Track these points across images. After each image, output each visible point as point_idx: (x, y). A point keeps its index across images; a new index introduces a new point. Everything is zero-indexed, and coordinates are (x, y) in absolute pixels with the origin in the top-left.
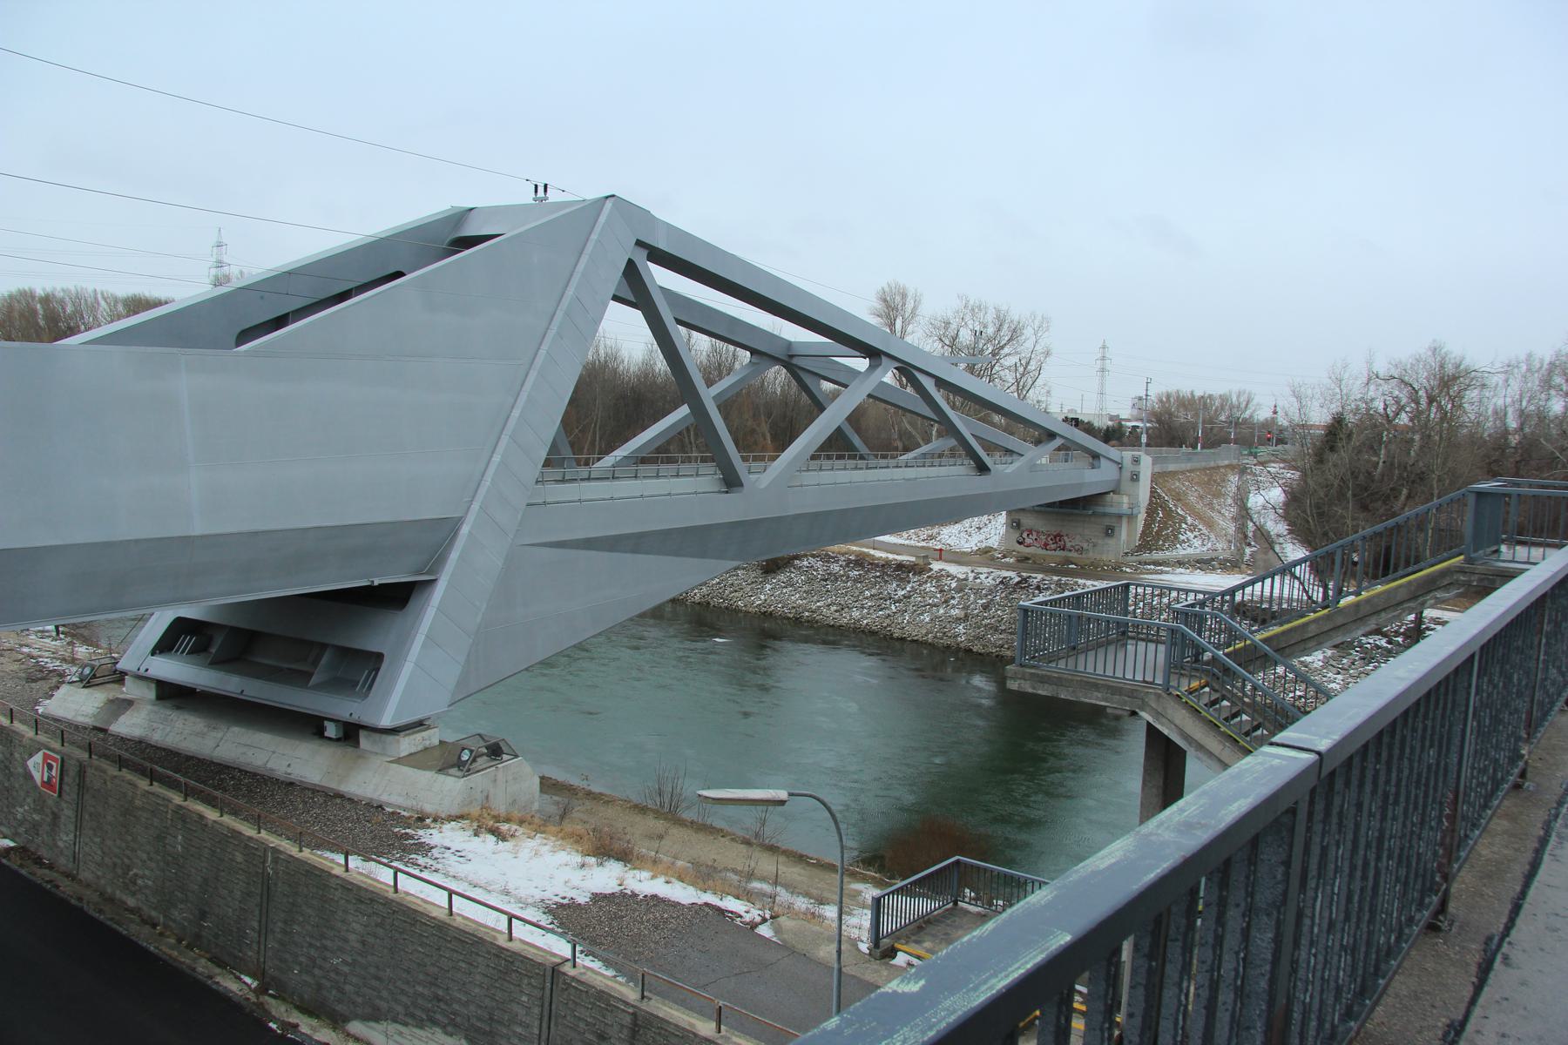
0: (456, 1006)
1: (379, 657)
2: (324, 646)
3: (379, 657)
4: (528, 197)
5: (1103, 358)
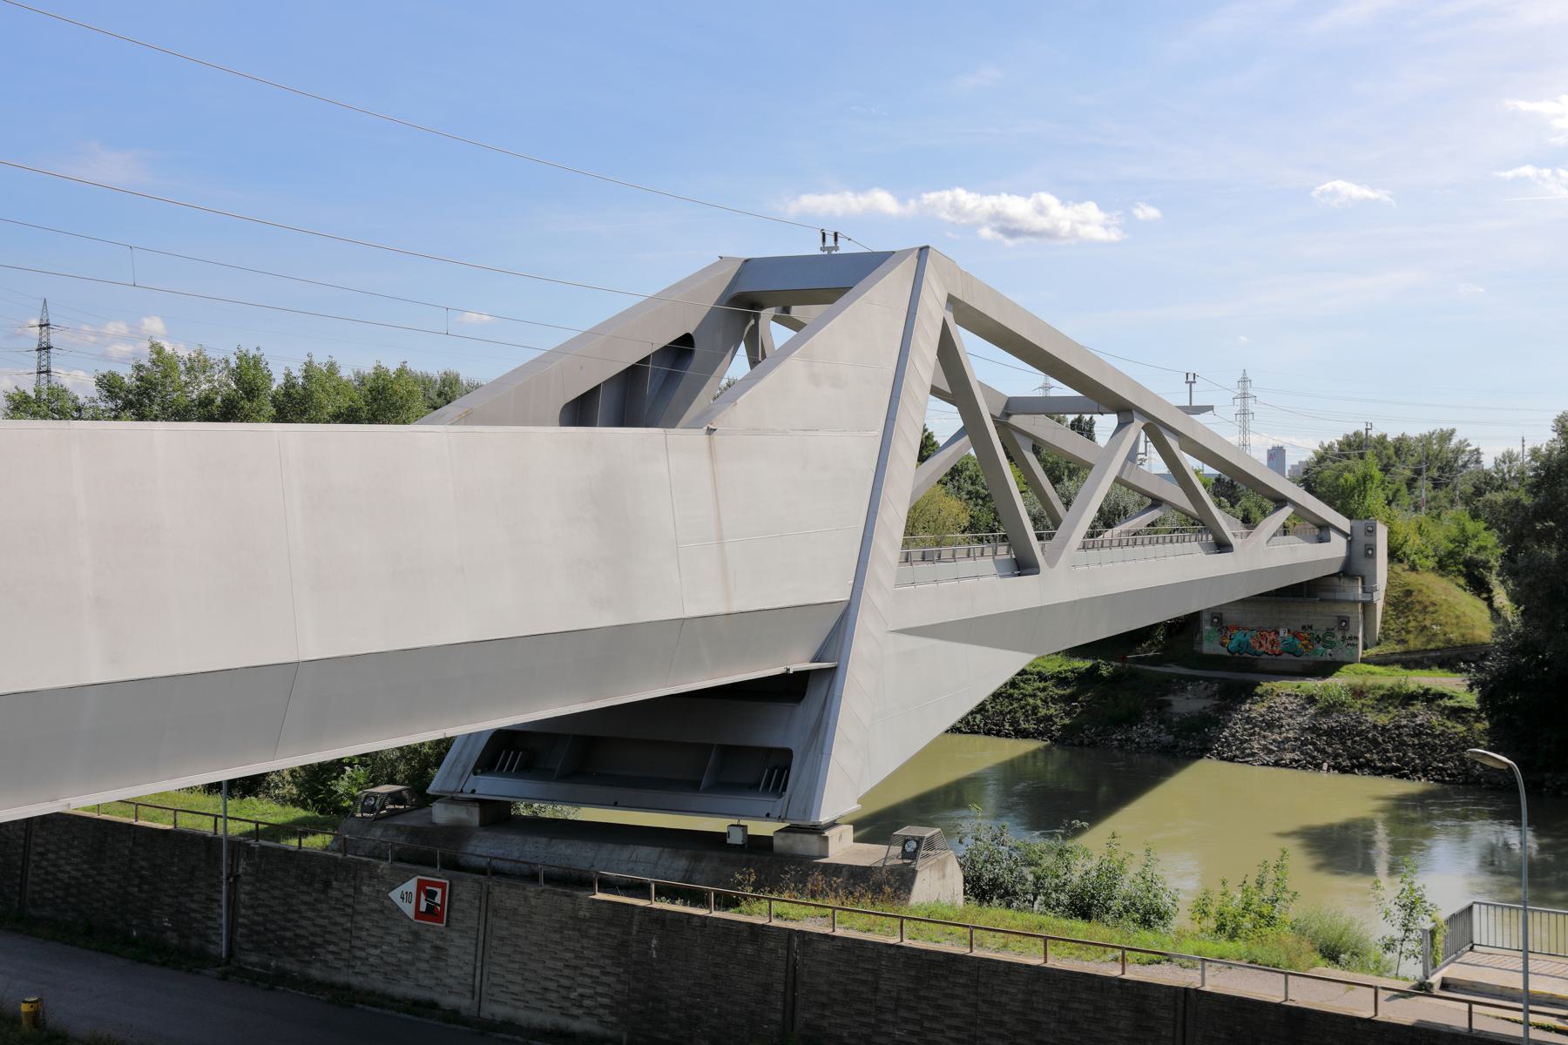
0: (927, 1024)
1: (788, 753)
2: (707, 748)
3: (788, 753)
4: (814, 249)
5: (1244, 396)
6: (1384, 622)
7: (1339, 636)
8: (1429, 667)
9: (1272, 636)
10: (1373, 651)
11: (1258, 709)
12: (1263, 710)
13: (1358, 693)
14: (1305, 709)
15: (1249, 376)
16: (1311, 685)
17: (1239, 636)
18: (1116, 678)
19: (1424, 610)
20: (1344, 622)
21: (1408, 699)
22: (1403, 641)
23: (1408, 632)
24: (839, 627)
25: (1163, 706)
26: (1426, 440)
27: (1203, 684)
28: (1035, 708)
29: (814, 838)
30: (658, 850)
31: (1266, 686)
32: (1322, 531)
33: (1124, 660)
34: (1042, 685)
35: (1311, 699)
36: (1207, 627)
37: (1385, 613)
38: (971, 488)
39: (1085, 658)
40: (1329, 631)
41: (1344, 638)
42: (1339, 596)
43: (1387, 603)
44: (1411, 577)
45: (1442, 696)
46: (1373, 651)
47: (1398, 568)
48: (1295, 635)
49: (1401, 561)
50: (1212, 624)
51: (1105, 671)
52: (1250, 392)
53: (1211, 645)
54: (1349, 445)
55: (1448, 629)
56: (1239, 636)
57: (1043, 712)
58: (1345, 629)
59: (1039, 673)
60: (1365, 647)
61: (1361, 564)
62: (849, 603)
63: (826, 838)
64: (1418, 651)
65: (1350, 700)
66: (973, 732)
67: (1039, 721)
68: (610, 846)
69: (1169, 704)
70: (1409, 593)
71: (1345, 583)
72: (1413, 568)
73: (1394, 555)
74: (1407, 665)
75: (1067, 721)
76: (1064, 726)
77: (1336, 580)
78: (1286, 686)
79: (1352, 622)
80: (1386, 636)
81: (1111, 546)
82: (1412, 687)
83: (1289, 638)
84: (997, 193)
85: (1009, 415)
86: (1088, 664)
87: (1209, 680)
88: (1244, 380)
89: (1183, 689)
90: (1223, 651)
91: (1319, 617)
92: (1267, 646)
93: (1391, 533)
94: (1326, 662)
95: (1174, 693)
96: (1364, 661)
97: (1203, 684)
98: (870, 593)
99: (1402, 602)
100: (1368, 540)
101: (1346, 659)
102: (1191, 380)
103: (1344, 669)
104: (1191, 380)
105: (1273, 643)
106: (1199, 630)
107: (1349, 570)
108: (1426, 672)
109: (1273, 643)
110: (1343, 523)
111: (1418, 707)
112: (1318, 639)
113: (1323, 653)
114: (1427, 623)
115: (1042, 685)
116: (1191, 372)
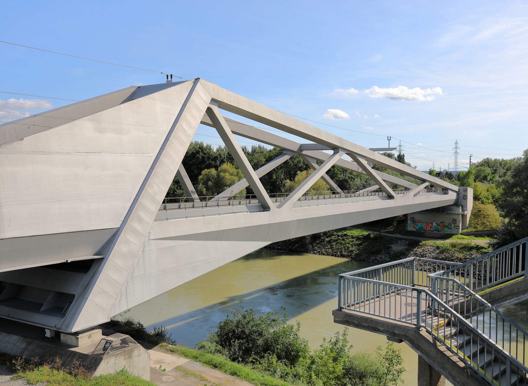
3: (73, 296)
5: (456, 148)
6: (470, 221)
7: (453, 225)
8: (484, 237)
9: (431, 225)
10: (465, 231)
11: (419, 250)
12: (421, 251)
13: (453, 246)
14: (435, 251)
15: (458, 142)
16: (439, 242)
17: (420, 225)
18: (376, 238)
19: (484, 217)
20: (455, 221)
21: (470, 248)
22: (476, 228)
23: (478, 224)
24: (110, 240)
25: (389, 248)
26: (511, 161)
27: (403, 241)
28: (348, 247)
29: (73, 337)
30: (19, 337)
31: (424, 242)
32: (445, 190)
33: (380, 232)
34: (352, 240)
35: (438, 248)
36: (409, 222)
37: (471, 218)
38: (349, 175)
39: (367, 230)
40: (450, 224)
41: (455, 226)
42: (453, 212)
43: (472, 214)
44: (482, 206)
45: (482, 248)
46: (465, 231)
47: (477, 203)
48: (438, 225)
49: (479, 200)
50: (411, 221)
51: (372, 236)
52: (458, 146)
53: (410, 227)
54: (485, 162)
55: (492, 224)
56: (420, 225)
57: (351, 249)
58: (455, 223)
59: (352, 236)
60: (462, 229)
61: (462, 201)
62: (119, 229)
63: (78, 338)
64: (481, 231)
65: (451, 248)
66: (328, 255)
67: (349, 252)
68: (4, 334)
69: (391, 247)
70: (480, 211)
71: (455, 208)
72: (483, 203)
73: (476, 198)
74: (476, 236)
75: (357, 252)
76: (356, 254)
77: (452, 207)
78: (431, 242)
79: (457, 221)
80: (470, 225)
81: (363, 196)
82: (473, 244)
83: (436, 226)
84: (389, 88)
85: (302, 151)
86: (367, 233)
87: (406, 239)
88: (456, 143)
89: (397, 243)
90: (414, 230)
91: (446, 219)
92: (429, 228)
93: (475, 191)
94: (449, 234)
95: (394, 244)
96: (461, 234)
97: (403, 241)
98: (133, 223)
99: (476, 214)
100: (465, 193)
101: (456, 233)
102: (389, 139)
103: (454, 237)
104: (389, 139)
105: (431, 227)
106: (407, 222)
107: (457, 204)
108: (483, 238)
109: (431, 227)
110: (456, 188)
111: (474, 251)
112: (446, 227)
113: (447, 231)
114: (485, 221)
115: (352, 240)
116: (389, 136)
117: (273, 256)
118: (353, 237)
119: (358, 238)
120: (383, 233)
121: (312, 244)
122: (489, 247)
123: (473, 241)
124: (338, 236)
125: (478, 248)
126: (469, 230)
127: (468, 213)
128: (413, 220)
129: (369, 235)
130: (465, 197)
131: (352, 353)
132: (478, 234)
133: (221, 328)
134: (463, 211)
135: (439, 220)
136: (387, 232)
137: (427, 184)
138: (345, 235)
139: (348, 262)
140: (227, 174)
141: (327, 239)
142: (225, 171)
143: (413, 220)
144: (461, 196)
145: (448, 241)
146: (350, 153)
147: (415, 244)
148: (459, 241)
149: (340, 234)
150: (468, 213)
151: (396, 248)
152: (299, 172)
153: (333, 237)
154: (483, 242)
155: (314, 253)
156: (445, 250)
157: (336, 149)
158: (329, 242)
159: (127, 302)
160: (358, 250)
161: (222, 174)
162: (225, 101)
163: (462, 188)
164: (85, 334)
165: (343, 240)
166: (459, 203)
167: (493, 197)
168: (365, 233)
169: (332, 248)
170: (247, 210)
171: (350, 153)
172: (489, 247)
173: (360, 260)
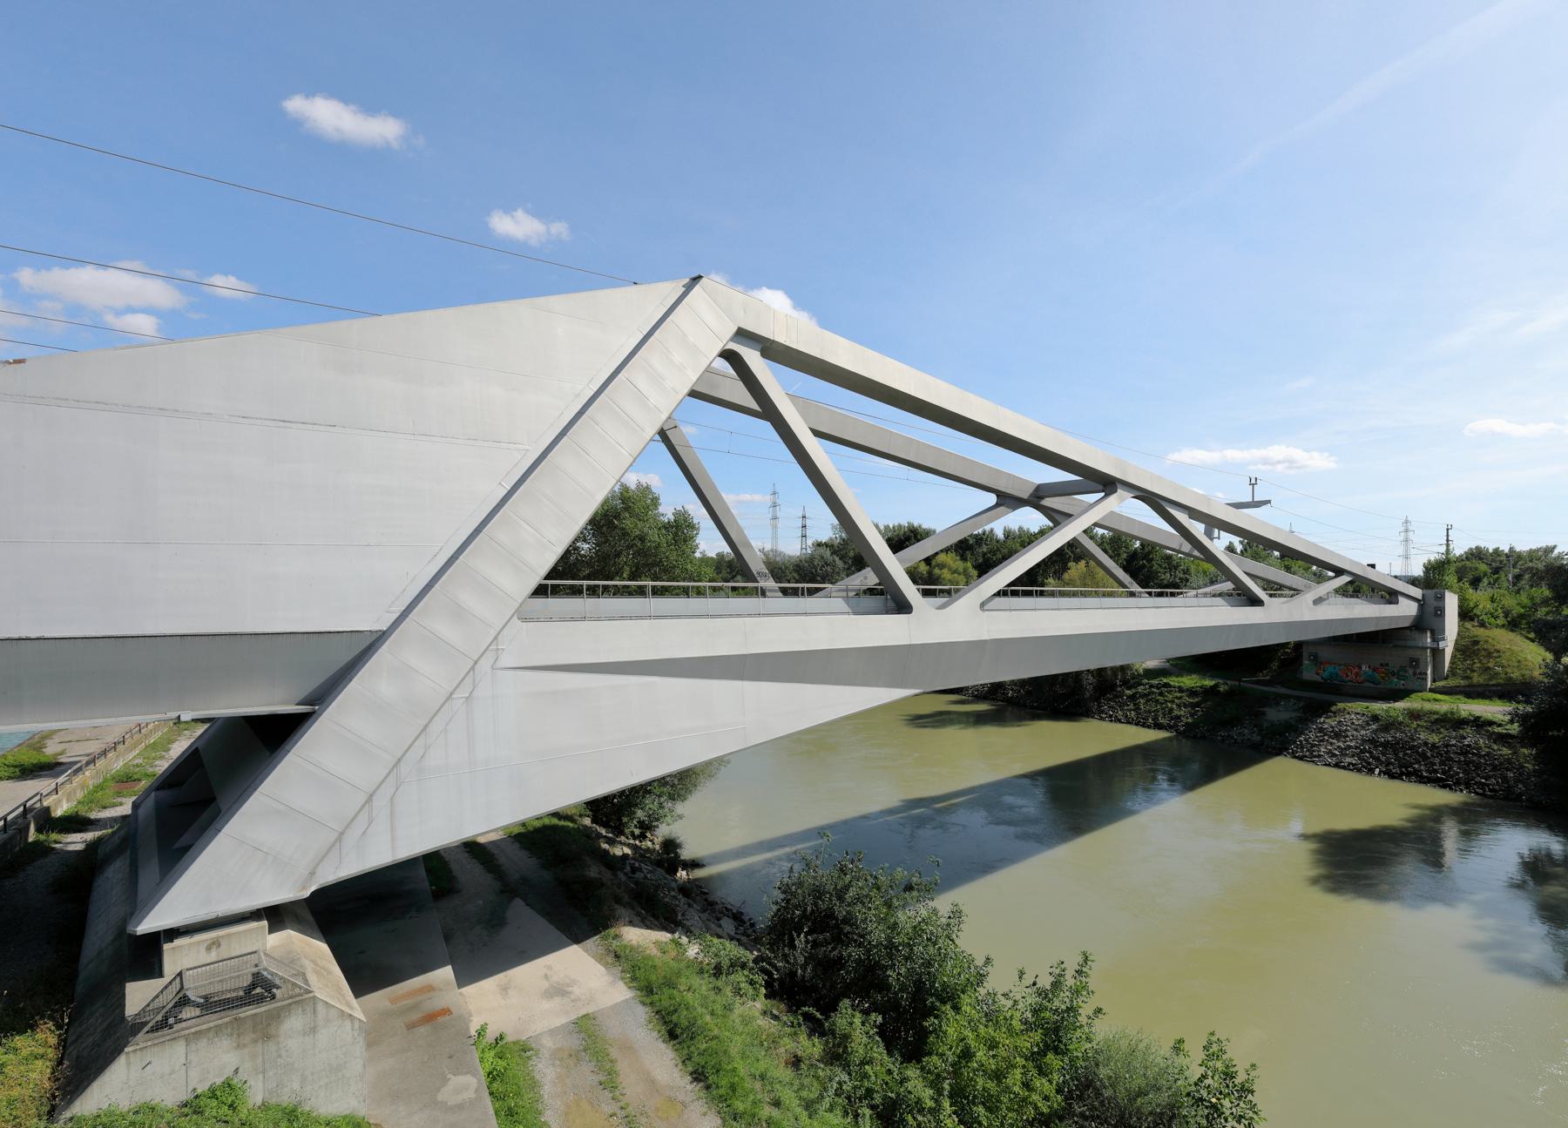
5: (1407, 531)
6: (1452, 663)
7: (1411, 671)
11: (1329, 723)
13: (1414, 715)
16: (1379, 707)
18: (1230, 694)
20: (1415, 663)
22: (1467, 678)
28: (1171, 710)
35: (1375, 718)
37: (1453, 657)
40: (1403, 668)
43: (1457, 648)
44: (1480, 632)
45: (1491, 723)
47: (1468, 625)
48: (1375, 670)
53: (1309, 673)
57: (1176, 712)
60: (1434, 681)
65: (1407, 720)
69: (1264, 713)
70: (1476, 643)
71: (1416, 634)
73: (1465, 614)
78: (1359, 706)
80: (1453, 671)
82: (1464, 714)
87: (1299, 698)
89: (1278, 704)
90: (1318, 678)
92: (1352, 676)
96: (1431, 690)
98: (430, 618)
99: (1466, 648)
102: (1253, 483)
104: (1253, 483)
105: (1357, 674)
109: (1357, 674)
112: (1393, 674)
113: (1401, 684)
117: (1024, 719)
118: (1181, 690)
119: (1192, 692)
120: (1247, 683)
121: (1097, 700)
122: (1512, 722)
123: (1462, 706)
124: (1152, 686)
125: (1479, 724)
126: (1451, 682)
127: (1449, 646)
128: (1315, 659)
129: (1216, 686)
130: (1440, 612)
131: (1102, 1030)
132: (1473, 693)
133: (785, 889)
134: (1434, 640)
135: (1376, 658)
136: (1258, 682)
137: (1345, 579)
138: (1167, 685)
139: (1169, 739)
140: (945, 571)
141: (1128, 692)
142: (942, 566)
143: (1315, 659)
144: (1430, 610)
145: (1400, 705)
146: (1155, 501)
147: (1324, 709)
148: (1428, 706)
149: (1155, 682)
150: (1449, 646)
151: (1276, 715)
152: (1071, 564)
153: (1140, 689)
154: (1494, 710)
155: (1102, 719)
156: (1392, 724)
157: (1108, 484)
158: (1132, 698)
159: (393, 839)
160: (1192, 715)
161: (937, 571)
162: (781, 338)
163: (1430, 593)
164: (198, 937)
165: (1161, 694)
166: (1428, 621)
167: (1506, 615)
168: (1209, 683)
169: (1137, 709)
170: (847, 609)
171: (1155, 501)
172: (1512, 722)
173: (1195, 737)
